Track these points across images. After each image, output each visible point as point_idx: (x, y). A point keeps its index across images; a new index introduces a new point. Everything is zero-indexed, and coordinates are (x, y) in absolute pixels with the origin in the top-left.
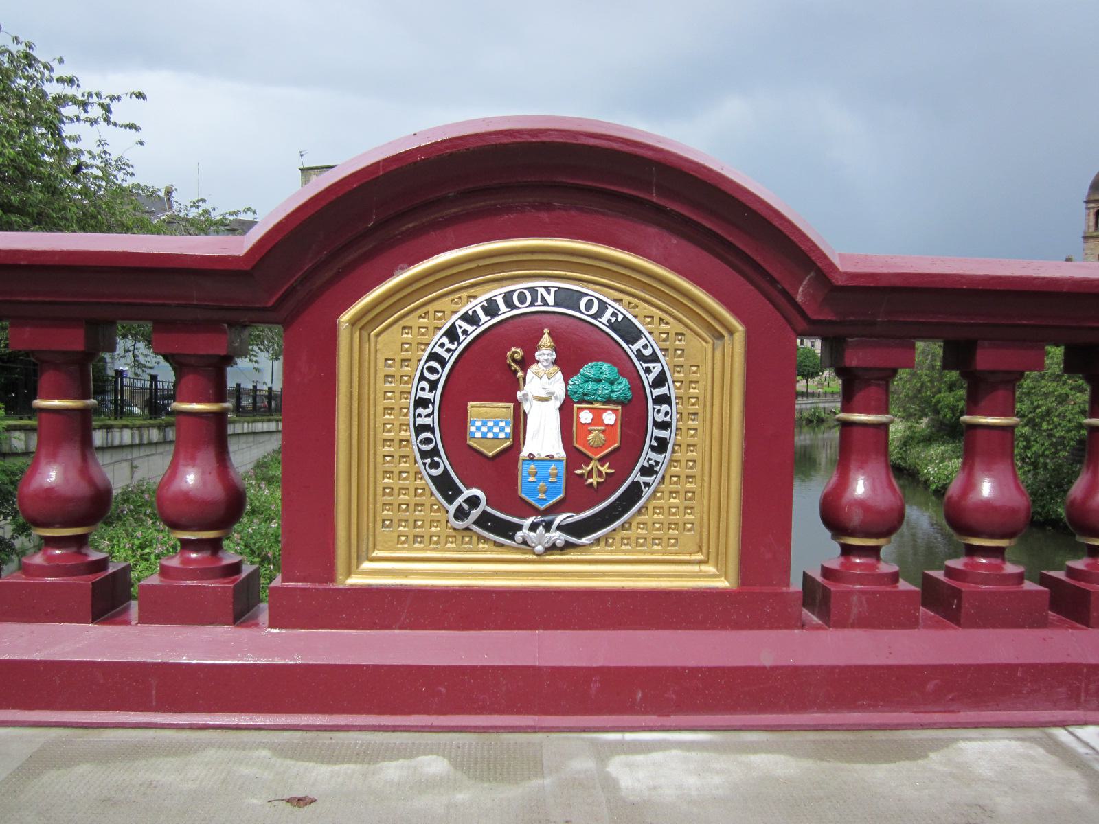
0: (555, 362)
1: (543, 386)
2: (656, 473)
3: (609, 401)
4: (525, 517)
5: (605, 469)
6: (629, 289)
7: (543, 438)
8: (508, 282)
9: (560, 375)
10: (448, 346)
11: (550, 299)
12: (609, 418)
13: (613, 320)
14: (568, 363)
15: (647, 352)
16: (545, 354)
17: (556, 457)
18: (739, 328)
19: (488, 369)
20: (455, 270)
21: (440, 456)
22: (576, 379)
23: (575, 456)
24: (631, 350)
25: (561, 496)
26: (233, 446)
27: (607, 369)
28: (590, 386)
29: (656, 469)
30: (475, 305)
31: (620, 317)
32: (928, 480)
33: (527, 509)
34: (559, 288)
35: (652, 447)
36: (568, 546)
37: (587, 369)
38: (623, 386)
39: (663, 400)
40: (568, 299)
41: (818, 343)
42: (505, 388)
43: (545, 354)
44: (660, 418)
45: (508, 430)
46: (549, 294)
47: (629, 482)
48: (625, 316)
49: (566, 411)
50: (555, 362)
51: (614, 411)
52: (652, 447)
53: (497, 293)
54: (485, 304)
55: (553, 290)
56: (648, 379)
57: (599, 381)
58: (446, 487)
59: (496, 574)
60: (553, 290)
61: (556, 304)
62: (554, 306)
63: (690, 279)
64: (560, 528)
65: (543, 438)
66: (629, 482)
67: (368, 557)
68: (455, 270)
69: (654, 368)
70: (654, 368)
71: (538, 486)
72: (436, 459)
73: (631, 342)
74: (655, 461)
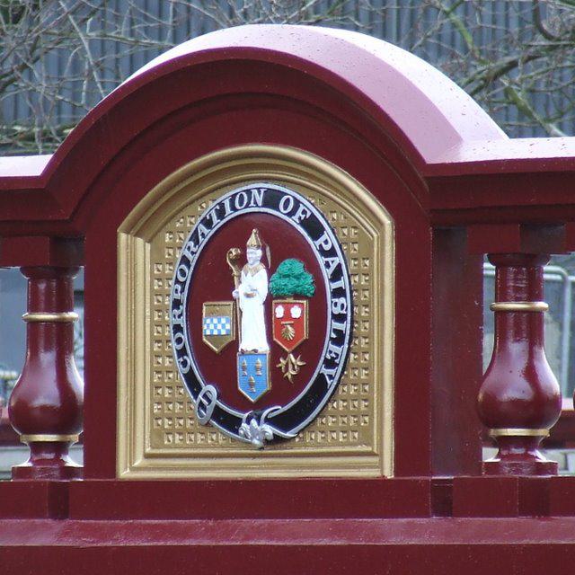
1: (253, 283)
2: (338, 365)
4: (245, 412)
6: (220, 183)
7: (254, 338)
8: (222, 190)
10: (193, 249)
11: (260, 200)
12: (296, 312)
13: (303, 217)
15: (327, 248)
16: (254, 254)
17: (260, 351)
18: (387, 221)
19: (211, 281)
20: (187, 183)
21: (187, 356)
23: (276, 353)
24: (314, 245)
26: (312, 289)
29: (337, 361)
30: (195, 223)
31: (309, 214)
33: (243, 404)
34: (269, 189)
35: (331, 339)
36: (277, 440)
38: (307, 282)
39: (339, 293)
40: (272, 199)
41: (233, 250)
43: (254, 254)
44: (337, 311)
45: (228, 326)
46: (260, 194)
47: (315, 375)
48: (312, 214)
51: (301, 305)
52: (331, 339)
53: (225, 197)
54: (218, 207)
55: (262, 191)
56: (327, 274)
58: (194, 387)
59: (213, 468)
60: (262, 191)
61: (265, 205)
62: (262, 206)
63: (329, 159)
64: (268, 421)
65: (254, 338)
66: (315, 375)
69: (333, 262)
70: (333, 262)
71: (253, 380)
72: (185, 357)
73: (315, 237)
74: (335, 354)
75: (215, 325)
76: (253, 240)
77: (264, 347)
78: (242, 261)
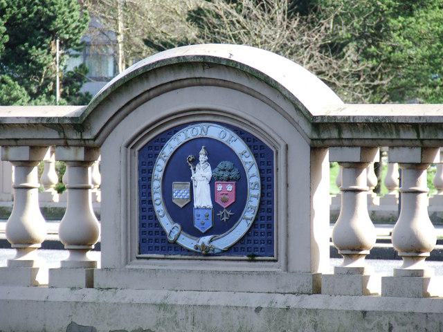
0: (208, 161)
1: (202, 173)
3: (228, 180)
5: (229, 213)
7: (203, 199)
9: (209, 168)
12: (230, 188)
14: (213, 162)
16: (203, 157)
22: (217, 169)
23: (217, 208)
25: (233, 201)
27: (228, 164)
28: (221, 173)
32: (411, 15)
37: (220, 166)
42: (186, 177)
43: (203, 157)
45: (188, 194)
49: (212, 183)
50: (208, 161)
57: (224, 170)
65: (203, 199)
67: (218, 180)
68: (162, 122)
75: (179, 194)
76: (203, 151)
77: (209, 204)
78: (196, 161)
